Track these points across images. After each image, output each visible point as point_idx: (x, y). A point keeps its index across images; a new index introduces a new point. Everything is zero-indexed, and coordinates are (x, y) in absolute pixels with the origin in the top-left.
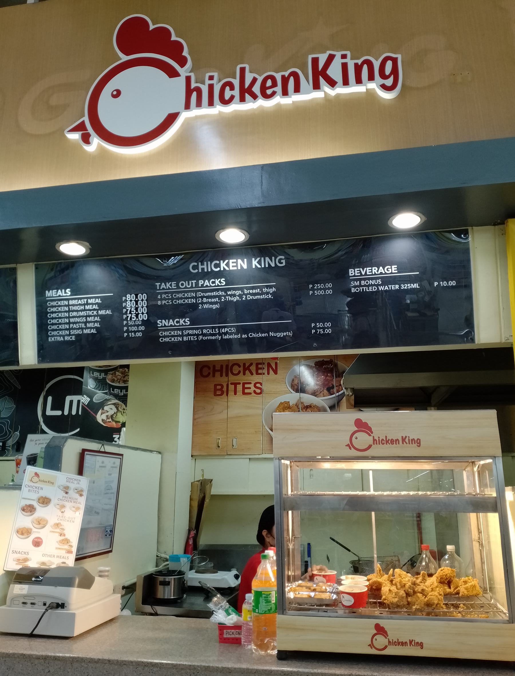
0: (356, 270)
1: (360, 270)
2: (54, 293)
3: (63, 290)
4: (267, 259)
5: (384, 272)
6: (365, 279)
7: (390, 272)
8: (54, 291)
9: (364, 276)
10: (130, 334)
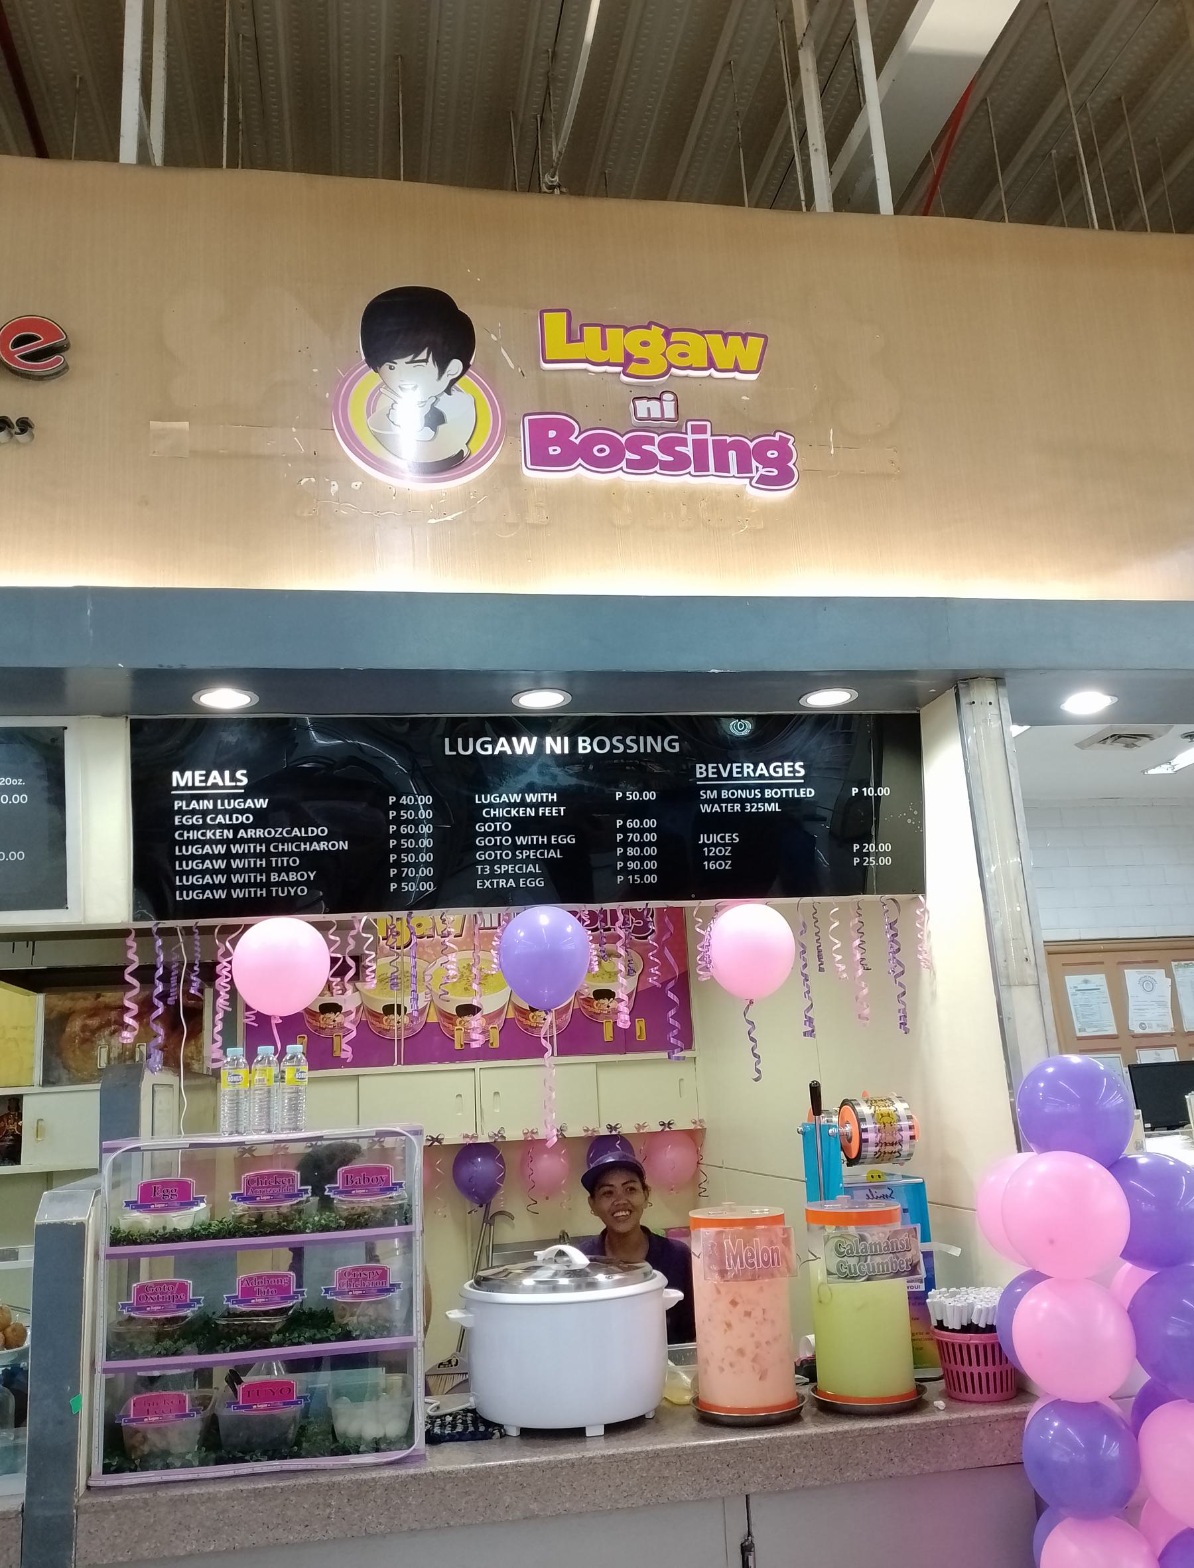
0: (710, 766)
1: (717, 768)
2: (197, 778)
3: (227, 773)
4: (650, 739)
5: (221, 784)
6: (728, 788)
7: (780, 774)
8: (197, 773)
9: (725, 779)
10: (274, 860)
